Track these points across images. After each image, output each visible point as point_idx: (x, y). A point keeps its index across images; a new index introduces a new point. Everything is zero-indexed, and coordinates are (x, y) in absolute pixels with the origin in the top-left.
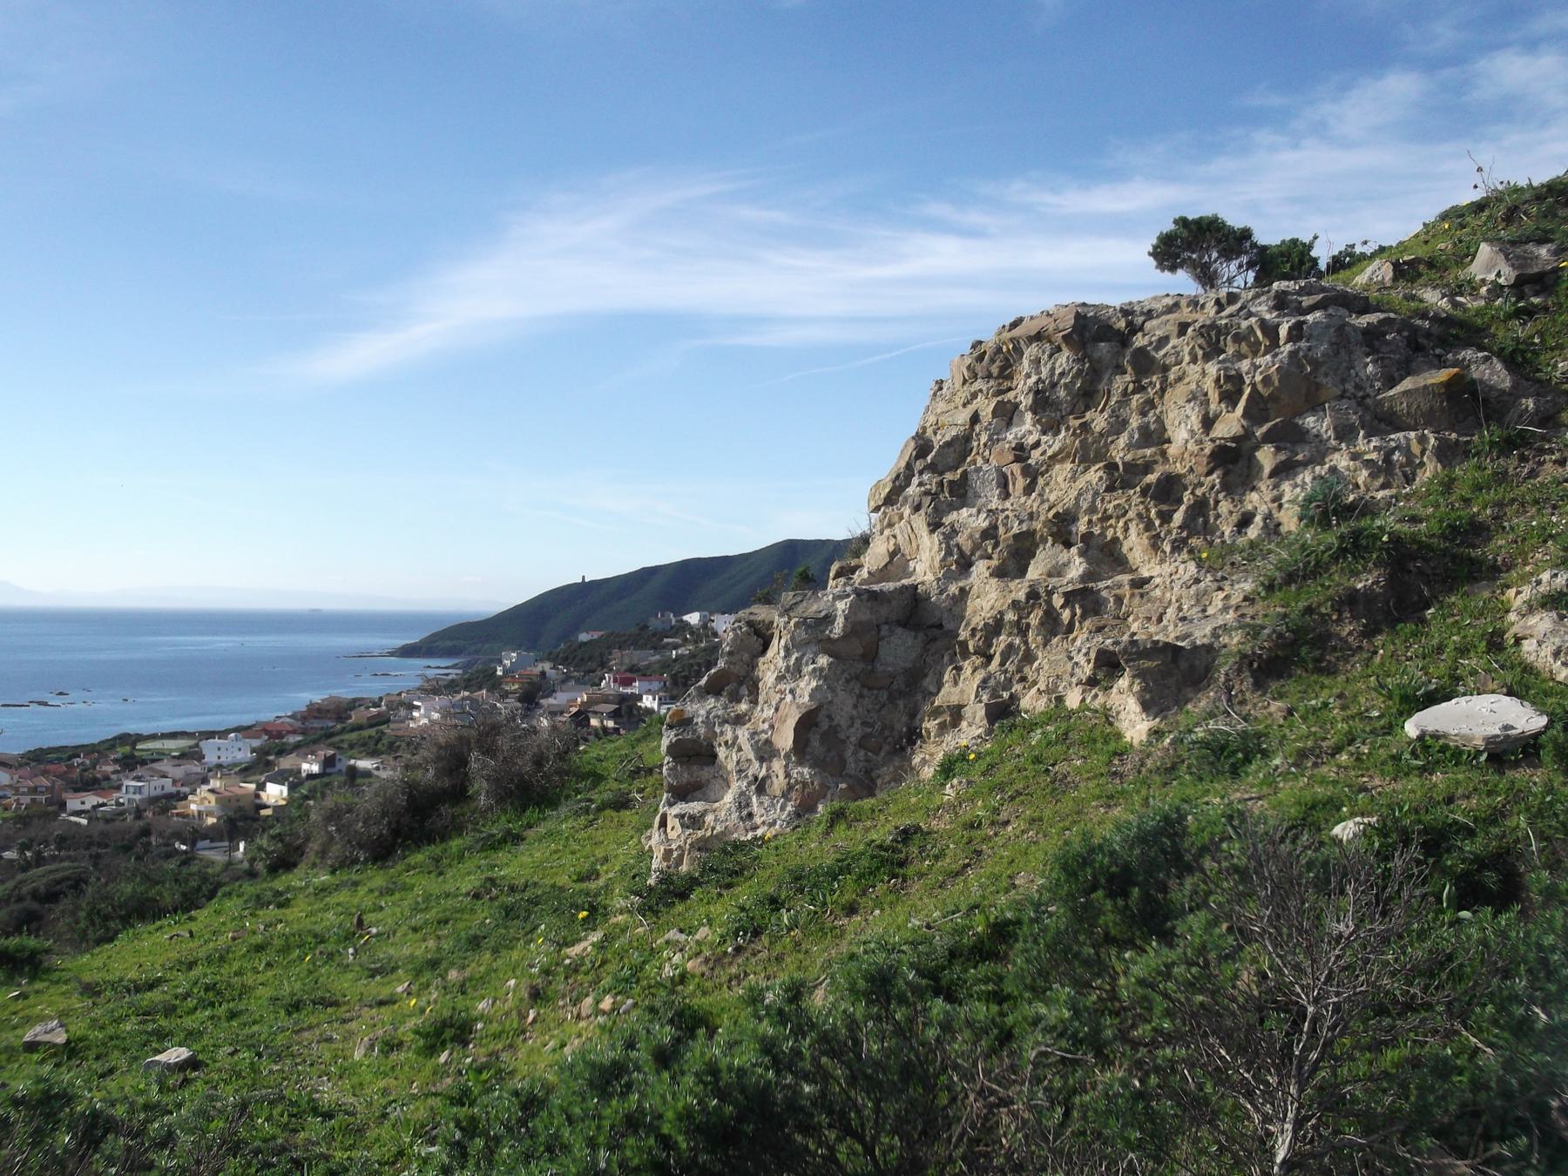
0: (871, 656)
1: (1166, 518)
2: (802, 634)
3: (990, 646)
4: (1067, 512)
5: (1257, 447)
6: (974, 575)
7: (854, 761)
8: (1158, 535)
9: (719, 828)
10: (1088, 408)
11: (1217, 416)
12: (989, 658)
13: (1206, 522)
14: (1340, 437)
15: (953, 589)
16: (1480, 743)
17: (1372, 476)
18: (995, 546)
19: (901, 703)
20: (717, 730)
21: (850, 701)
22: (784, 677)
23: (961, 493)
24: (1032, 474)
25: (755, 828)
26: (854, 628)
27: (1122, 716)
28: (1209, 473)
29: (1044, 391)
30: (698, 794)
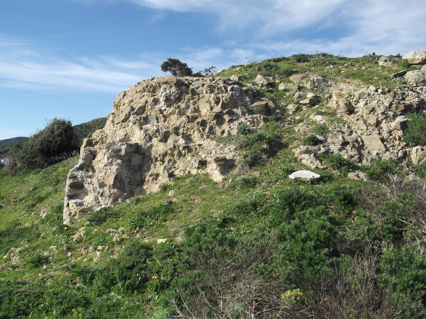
0: (129, 161)
1: (204, 130)
2: (113, 154)
3: (164, 159)
4: (177, 127)
5: (224, 115)
6: (153, 141)
7: (127, 188)
8: (202, 134)
9: (89, 206)
10: (179, 102)
11: (213, 107)
12: (164, 162)
13: (213, 132)
14: (242, 115)
15: (149, 144)
16: (309, 180)
17: (251, 124)
18: (159, 134)
19: (138, 173)
20: (85, 179)
21: (127, 172)
22: (107, 165)
23: (146, 120)
24: (165, 117)
25: (101, 205)
26: (127, 153)
27: (213, 175)
28: (213, 120)
29: (168, 96)
30: (76, 197)
